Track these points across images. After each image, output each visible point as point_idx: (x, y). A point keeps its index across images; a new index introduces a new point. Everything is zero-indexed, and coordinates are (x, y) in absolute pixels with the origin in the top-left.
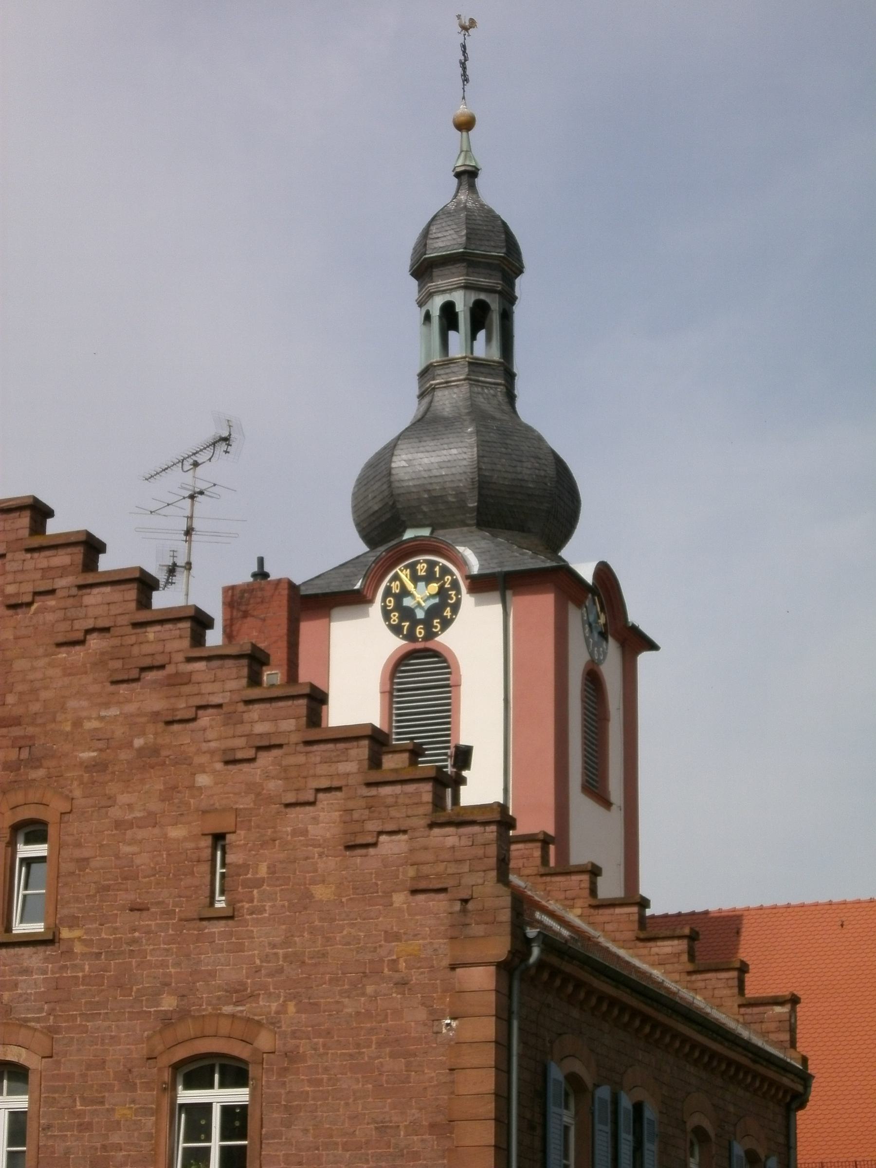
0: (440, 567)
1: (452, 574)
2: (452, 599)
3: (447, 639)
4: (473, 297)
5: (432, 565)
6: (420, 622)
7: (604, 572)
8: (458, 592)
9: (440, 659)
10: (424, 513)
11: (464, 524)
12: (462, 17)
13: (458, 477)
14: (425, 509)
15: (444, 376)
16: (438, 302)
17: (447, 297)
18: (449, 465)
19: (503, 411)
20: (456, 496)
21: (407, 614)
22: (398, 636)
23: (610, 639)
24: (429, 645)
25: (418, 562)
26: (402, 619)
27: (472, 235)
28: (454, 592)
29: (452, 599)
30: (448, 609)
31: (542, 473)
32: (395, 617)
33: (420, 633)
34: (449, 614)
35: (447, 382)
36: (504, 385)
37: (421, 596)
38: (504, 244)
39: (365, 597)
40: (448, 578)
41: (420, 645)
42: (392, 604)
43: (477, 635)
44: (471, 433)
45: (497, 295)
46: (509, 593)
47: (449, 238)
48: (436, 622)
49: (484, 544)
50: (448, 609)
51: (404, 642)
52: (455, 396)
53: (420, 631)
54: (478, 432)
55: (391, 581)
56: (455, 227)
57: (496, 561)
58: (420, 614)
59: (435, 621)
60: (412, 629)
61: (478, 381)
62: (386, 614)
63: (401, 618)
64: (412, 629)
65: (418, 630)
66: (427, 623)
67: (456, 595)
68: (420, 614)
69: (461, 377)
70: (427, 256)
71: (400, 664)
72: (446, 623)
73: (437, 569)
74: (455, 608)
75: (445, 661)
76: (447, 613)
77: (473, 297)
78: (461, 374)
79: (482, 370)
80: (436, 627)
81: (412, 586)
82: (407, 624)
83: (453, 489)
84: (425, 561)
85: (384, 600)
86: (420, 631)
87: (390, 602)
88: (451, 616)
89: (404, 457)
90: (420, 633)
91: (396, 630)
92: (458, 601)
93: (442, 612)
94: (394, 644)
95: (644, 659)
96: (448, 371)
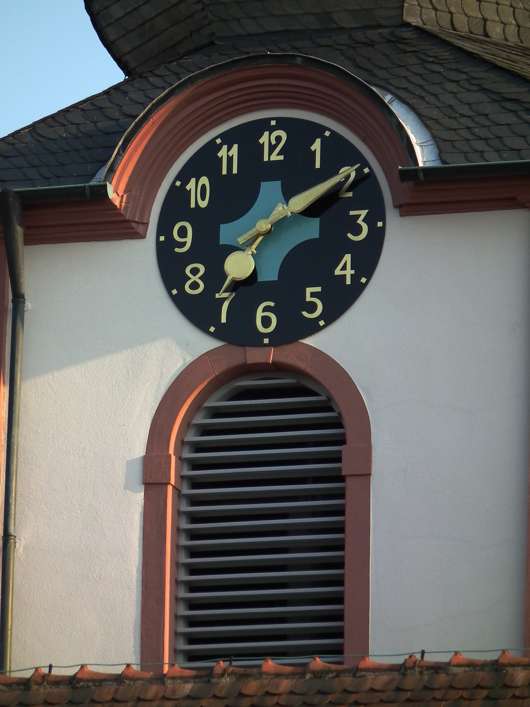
2: (358, 230)
5: (300, 134)
24: (286, 355)
25: (263, 125)
28: (363, 213)
30: (348, 258)
33: (266, 322)
34: (349, 272)
50: (348, 258)
51: (212, 344)
53: (264, 317)
55: (184, 175)
59: (309, 290)
60: (243, 312)
64: (243, 312)
72: (341, 300)
76: (345, 269)
84: (282, 124)
85: (164, 227)
87: (183, 232)
90: (266, 322)
92: (377, 238)
93: (328, 270)
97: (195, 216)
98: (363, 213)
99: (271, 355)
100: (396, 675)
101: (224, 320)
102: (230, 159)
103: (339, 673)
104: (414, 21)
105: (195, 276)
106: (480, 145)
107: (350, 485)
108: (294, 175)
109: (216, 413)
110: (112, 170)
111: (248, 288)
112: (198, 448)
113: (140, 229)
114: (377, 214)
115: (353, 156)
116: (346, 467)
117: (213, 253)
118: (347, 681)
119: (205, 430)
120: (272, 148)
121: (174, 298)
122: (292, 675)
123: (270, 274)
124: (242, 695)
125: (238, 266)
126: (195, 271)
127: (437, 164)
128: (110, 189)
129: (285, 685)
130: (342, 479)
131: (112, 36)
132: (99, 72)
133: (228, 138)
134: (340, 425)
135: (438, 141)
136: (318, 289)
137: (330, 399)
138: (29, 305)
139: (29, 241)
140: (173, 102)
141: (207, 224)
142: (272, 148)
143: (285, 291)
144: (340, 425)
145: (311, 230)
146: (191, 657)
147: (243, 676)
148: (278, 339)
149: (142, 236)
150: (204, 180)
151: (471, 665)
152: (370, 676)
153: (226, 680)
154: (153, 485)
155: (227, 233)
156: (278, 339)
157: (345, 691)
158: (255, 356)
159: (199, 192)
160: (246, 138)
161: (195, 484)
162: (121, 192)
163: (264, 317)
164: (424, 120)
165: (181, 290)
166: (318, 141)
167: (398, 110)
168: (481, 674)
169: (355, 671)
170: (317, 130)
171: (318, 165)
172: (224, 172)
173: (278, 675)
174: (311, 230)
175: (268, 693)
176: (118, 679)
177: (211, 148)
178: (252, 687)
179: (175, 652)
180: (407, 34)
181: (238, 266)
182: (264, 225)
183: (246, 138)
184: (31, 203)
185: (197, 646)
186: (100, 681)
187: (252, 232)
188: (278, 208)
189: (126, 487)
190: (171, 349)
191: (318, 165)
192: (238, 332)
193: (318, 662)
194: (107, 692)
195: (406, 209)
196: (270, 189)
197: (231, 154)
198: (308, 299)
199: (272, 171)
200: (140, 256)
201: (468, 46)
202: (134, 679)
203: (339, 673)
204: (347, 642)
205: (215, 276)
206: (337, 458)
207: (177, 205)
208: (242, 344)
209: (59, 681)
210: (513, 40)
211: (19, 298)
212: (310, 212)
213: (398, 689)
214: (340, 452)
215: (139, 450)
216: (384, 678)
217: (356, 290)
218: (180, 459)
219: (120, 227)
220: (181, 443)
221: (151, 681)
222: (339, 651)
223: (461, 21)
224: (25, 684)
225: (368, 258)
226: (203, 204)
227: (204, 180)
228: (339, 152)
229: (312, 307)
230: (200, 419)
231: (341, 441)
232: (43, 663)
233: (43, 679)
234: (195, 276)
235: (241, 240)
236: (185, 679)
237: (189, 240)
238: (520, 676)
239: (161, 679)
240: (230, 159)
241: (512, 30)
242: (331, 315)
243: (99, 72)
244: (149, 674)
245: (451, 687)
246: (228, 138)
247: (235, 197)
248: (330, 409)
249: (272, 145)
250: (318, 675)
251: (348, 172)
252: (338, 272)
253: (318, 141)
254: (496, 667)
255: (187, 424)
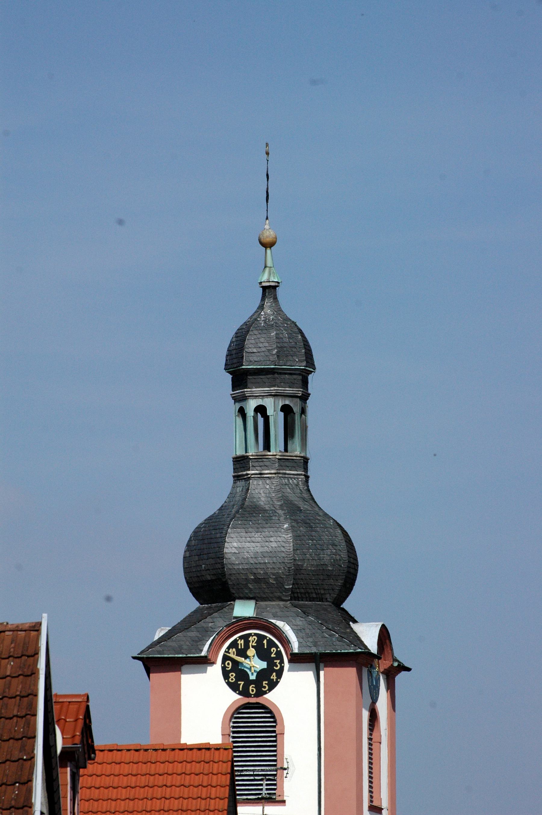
1: (277, 647)
2: (277, 666)
3: (273, 697)
4: (281, 403)
6: (252, 682)
8: (282, 662)
9: (270, 714)
10: (251, 590)
11: (280, 599)
13: (278, 565)
14: (250, 586)
15: (259, 468)
16: (251, 405)
17: (259, 402)
18: (271, 555)
19: (304, 499)
20: (275, 579)
21: (242, 675)
22: (235, 692)
26: (238, 678)
27: (282, 352)
28: (278, 661)
29: (277, 666)
30: (274, 674)
31: (338, 557)
32: (232, 676)
33: (253, 691)
34: (275, 678)
35: (261, 474)
36: (304, 475)
37: (255, 664)
38: (304, 358)
39: (210, 660)
40: (273, 649)
41: (253, 700)
42: (230, 666)
43: (296, 695)
44: (287, 529)
45: (298, 400)
46: (322, 665)
47: (262, 354)
48: (265, 683)
49: (300, 621)
50: (274, 674)
51: (240, 697)
52: (268, 487)
53: (252, 689)
54: (292, 528)
56: (267, 345)
57: (311, 640)
58: (253, 677)
59: (264, 682)
60: (246, 687)
61: (285, 474)
62: (226, 674)
63: (235, 677)
64: (246, 687)
65: (251, 688)
66: (258, 683)
68: (253, 677)
69: (273, 472)
70: (243, 367)
71: (237, 713)
72: (273, 685)
74: (280, 673)
75: (273, 717)
76: (274, 677)
77: (281, 403)
78: (273, 469)
79: (287, 464)
80: (265, 687)
82: (243, 683)
83: (273, 574)
84: (256, 634)
85: (223, 662)
86: (252, 689)
88: (277, 679)
89: (235, 544)
90: (253, 691)
91: (233, 687)
92: (282, 669)
93: (269, 678)
94: (231, 698)
96: (261, 464)
98: (278, 661)
101: (241, 689)
102: (241, 644)
120: (253, 642)
121: (269, 692)
126: (232, 675)
136: (267, 682)
142: (253, 642)
149: (213, 663)
150: (234, 650)
165: (228, 680)
166: (265, 640)
170: (265, 637)
171: (266, 647)
172: (240, 647)
177: (236, 641)
183: (246, 638)
191: (266, 647)
197: (241, 642)
198: (264, 685)
200: (215, 671)
208: (248, 697)
214: (233, 391)
217: (277, 683)
227: (234, 650)
240: (241, 644)
242: (270, 690)
246: (241, 638)
252: (272, 678)
253: (265, 640)
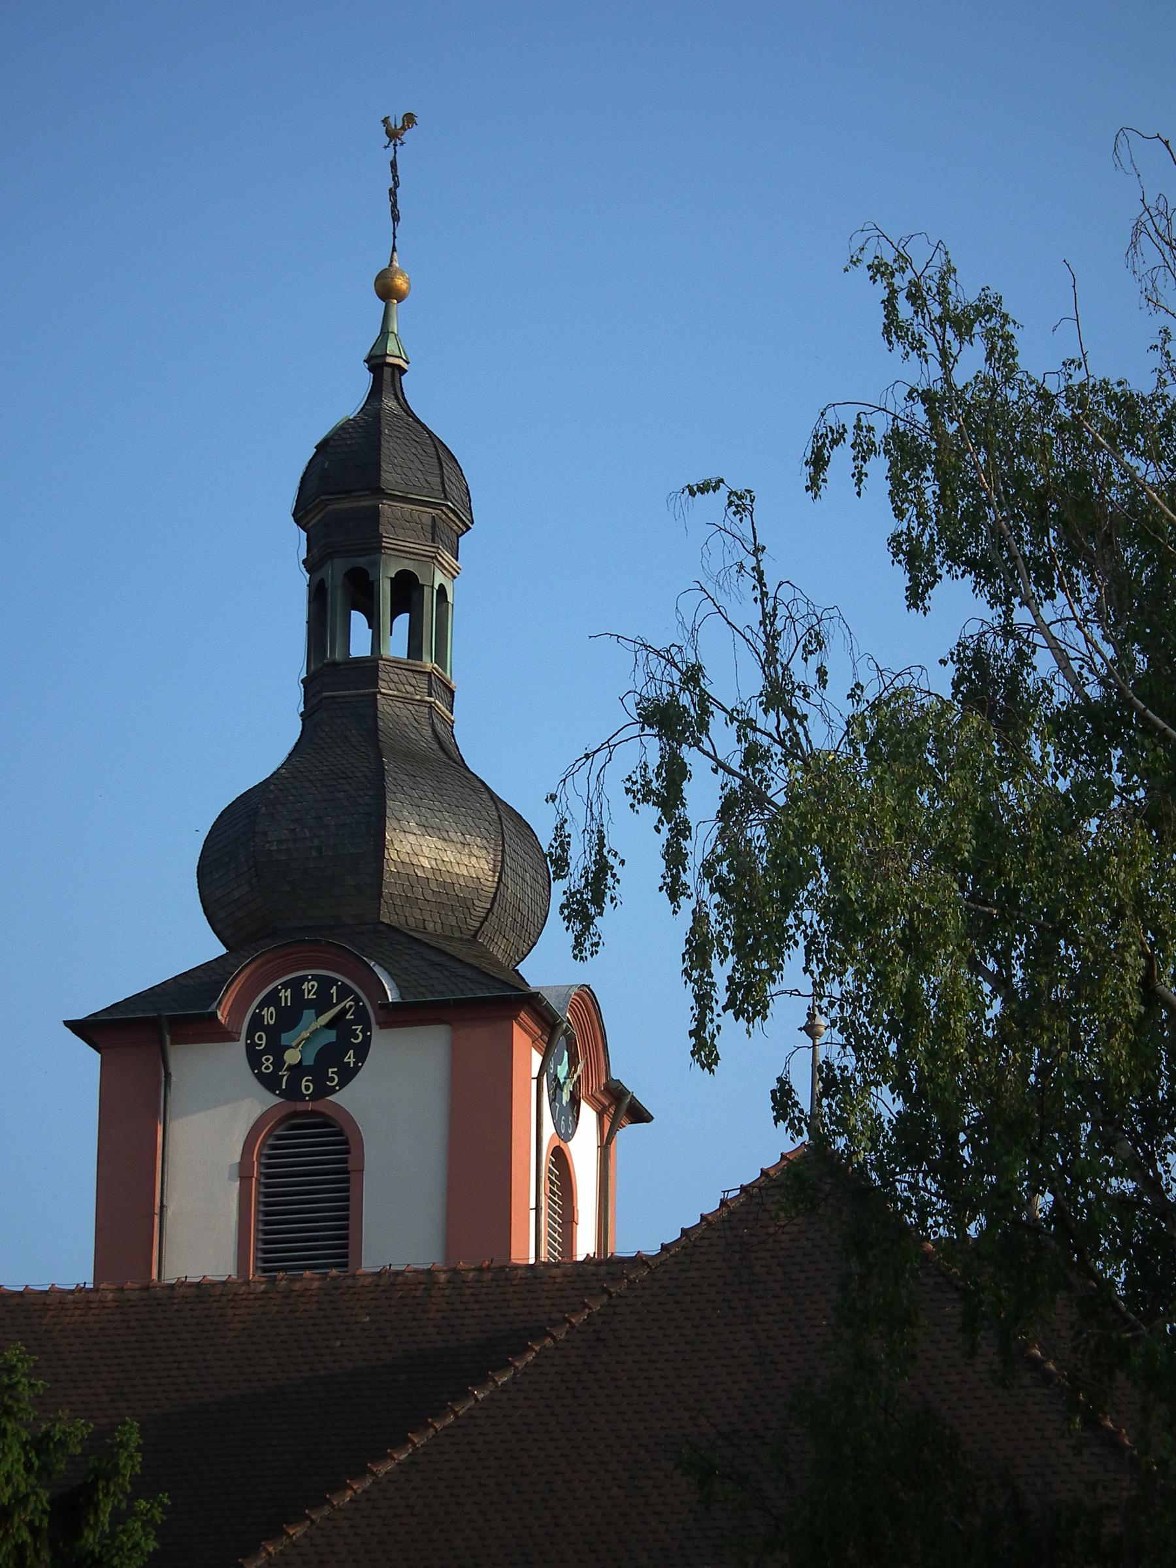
0: (338, 987)
2: (357, 1037)
5: (325, 984)
7: (737, 1019)
12: (391, 121)
23: (583, 1104)
24: (319, 1106)
25: (304, 979)
30: (351, 1052)
33: (307, 1088)
34: (352, 1060)
50: (351, 1052)
53: (306, 1085)
55: (261, 1006)
60: (294, 1082)
64: (294, 1082)
67: (363, 1031)
72: (347, 1075)
73: (334, 990)
75: (340, 1133)
81: (323, 1023)
85: (250, 1035)
87: (260, 1038)
90: (307, 1088)
92: (367, 1041)
93: (340, 1058)
95: (629, 1133)
97: (268, 1029)
99: (310, 1106)
100: (375, 1277)
102: (286, 997)
103: (345, 1278)
104: (386, 921)
105: (268, 1062)
106: (423, 990)
107: (352, 1176)
108: (321, 1004)
109: (280, 1138)
110: (220, 1003)
111: (298, 1070)
112: (270, 1157)
113: (236, 1036)
114: (367, 1028)
115: (350, 991)
116: (350, 1166)
117: (277, 1049)
118: (349, 1282)
119: (274, 1147)
120: (309, 992)
122: (318, 1280)
123: (309, 1061)
124: (292, 1291)
125: (292, 1057)
127: (400, 1000)
128: (219, 1014)
129: (316, 1284)
130: (348, 1173)
131: (219, 928)
132: (208, 947)
133: (285, 985)
134: (347, 1144)
135: (401, 988)
137: (342, 1129)
138: (173, 1079)
139: (173, 1043)
140: (263, 959)
141: (273, 1034)
142: (309, 992)
143: (317, 1071)
144: (347, 1144)
145: (331, 1036)
146: (265, 1270)
147: (293, 1280)
148: (314, 1097)
150: (272, 1009)
151: (416, 1271)
152: (362, 1278)
153: (284, 1282)
154: (244, 1178)
155: (285, 1038)
156: (314, 1097)
157: (349, 1287)
158: (301, 1106)
159: (269, 1016)
160: (295, 985)
161: (268, 1176)
162: (226, 1013)
163: (306, 1085)
164: (392, 976)
165: (260, 1070)
167: (378, 970)
168: (421, 1276)
169: (354, 1276)
170: (334, 981)
173: (312, 1279)
174: (331, 1036)
175: (306, 1289)
176: (224, 1283)
177: (276, 991)
178: (297, 1286)
179: (256, 1268)
180: (382, 928)
181: (292, 1057)
182: (306, 1034)
183: (295, 985)
184: (174, 1021)
185: (268, 1265)
186: (214, 1284)
187: (299, 1039)
188: (313, 1023)
189: (230, 1178)
190: (253, 1104)
192: (292, 1093)
193: (334, 1272)
194: (217, 1291)
195: (383, 1025)
196: (308, 1014)
197: (286, 995)
199: (310, 1004)
200: (238, 1049)
201: (415, 935)
202: (233, 1283)
203: (345, 1278)
204: (351, 1260)
205: (279, 1063)
206: (345, 1161)
207: (257, 1023)
209: (192, 1285)
210: (439, 931)
211: (168, 1075)
212: (329, 1025)
213: (377, 1285)
215: (237, 1159)
216: (370, 1279)
217: (357, 1069)
218: (260, 1164)
219: (224, 1035)
220: (260, 1155)
221: (242, 1284)
222: (345, 1265)
223: (411, 921)
224: (172, 1286)
225: (362, 1052)
226: (272, 1023)
227: (272, 1009)
228: (344, 992)
229: (332, 1080)
230: (270, 1142)
231: (347, 1152)
232: (182, 1275)
233: (182, 1284)
234: (268, 1062)
235: (294, 1044)
236: (261, 1283)
237: (264, 1042)
238: (443, 1277)
239: (248, 1283)
240: (286, 997)
241: (439, 926)
242: (343, 1084)
243: (208, 947)
244: (241, 1281)
245: (405, 1284)
246: (285, 985)
247: (289, 1018)
248: (342, 1135)
249: (310, 990)
250: (334, 1278)
251: (348, 1003)
252: (346, 1060)
254: (429, 1272)
255: (263, 1144)
